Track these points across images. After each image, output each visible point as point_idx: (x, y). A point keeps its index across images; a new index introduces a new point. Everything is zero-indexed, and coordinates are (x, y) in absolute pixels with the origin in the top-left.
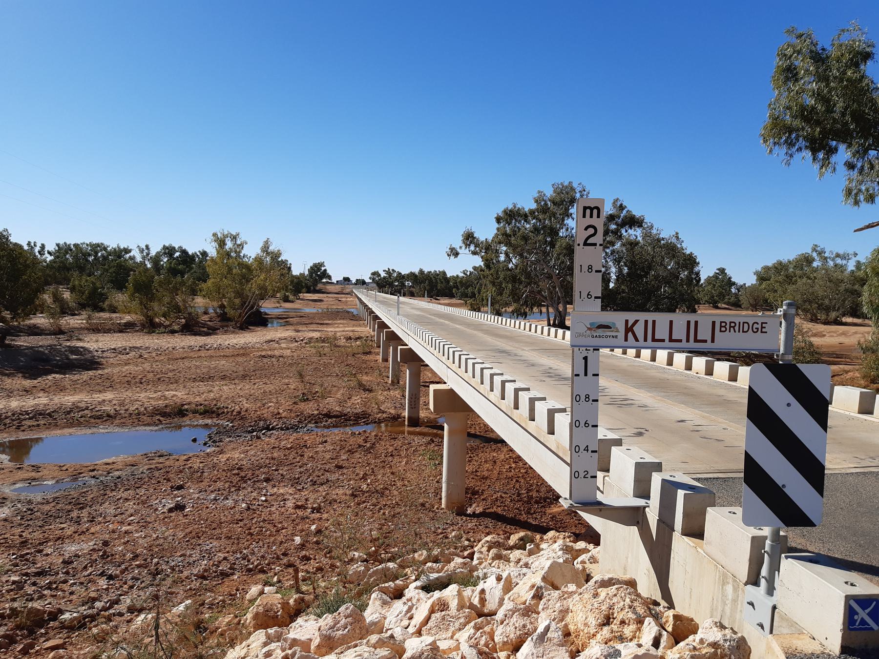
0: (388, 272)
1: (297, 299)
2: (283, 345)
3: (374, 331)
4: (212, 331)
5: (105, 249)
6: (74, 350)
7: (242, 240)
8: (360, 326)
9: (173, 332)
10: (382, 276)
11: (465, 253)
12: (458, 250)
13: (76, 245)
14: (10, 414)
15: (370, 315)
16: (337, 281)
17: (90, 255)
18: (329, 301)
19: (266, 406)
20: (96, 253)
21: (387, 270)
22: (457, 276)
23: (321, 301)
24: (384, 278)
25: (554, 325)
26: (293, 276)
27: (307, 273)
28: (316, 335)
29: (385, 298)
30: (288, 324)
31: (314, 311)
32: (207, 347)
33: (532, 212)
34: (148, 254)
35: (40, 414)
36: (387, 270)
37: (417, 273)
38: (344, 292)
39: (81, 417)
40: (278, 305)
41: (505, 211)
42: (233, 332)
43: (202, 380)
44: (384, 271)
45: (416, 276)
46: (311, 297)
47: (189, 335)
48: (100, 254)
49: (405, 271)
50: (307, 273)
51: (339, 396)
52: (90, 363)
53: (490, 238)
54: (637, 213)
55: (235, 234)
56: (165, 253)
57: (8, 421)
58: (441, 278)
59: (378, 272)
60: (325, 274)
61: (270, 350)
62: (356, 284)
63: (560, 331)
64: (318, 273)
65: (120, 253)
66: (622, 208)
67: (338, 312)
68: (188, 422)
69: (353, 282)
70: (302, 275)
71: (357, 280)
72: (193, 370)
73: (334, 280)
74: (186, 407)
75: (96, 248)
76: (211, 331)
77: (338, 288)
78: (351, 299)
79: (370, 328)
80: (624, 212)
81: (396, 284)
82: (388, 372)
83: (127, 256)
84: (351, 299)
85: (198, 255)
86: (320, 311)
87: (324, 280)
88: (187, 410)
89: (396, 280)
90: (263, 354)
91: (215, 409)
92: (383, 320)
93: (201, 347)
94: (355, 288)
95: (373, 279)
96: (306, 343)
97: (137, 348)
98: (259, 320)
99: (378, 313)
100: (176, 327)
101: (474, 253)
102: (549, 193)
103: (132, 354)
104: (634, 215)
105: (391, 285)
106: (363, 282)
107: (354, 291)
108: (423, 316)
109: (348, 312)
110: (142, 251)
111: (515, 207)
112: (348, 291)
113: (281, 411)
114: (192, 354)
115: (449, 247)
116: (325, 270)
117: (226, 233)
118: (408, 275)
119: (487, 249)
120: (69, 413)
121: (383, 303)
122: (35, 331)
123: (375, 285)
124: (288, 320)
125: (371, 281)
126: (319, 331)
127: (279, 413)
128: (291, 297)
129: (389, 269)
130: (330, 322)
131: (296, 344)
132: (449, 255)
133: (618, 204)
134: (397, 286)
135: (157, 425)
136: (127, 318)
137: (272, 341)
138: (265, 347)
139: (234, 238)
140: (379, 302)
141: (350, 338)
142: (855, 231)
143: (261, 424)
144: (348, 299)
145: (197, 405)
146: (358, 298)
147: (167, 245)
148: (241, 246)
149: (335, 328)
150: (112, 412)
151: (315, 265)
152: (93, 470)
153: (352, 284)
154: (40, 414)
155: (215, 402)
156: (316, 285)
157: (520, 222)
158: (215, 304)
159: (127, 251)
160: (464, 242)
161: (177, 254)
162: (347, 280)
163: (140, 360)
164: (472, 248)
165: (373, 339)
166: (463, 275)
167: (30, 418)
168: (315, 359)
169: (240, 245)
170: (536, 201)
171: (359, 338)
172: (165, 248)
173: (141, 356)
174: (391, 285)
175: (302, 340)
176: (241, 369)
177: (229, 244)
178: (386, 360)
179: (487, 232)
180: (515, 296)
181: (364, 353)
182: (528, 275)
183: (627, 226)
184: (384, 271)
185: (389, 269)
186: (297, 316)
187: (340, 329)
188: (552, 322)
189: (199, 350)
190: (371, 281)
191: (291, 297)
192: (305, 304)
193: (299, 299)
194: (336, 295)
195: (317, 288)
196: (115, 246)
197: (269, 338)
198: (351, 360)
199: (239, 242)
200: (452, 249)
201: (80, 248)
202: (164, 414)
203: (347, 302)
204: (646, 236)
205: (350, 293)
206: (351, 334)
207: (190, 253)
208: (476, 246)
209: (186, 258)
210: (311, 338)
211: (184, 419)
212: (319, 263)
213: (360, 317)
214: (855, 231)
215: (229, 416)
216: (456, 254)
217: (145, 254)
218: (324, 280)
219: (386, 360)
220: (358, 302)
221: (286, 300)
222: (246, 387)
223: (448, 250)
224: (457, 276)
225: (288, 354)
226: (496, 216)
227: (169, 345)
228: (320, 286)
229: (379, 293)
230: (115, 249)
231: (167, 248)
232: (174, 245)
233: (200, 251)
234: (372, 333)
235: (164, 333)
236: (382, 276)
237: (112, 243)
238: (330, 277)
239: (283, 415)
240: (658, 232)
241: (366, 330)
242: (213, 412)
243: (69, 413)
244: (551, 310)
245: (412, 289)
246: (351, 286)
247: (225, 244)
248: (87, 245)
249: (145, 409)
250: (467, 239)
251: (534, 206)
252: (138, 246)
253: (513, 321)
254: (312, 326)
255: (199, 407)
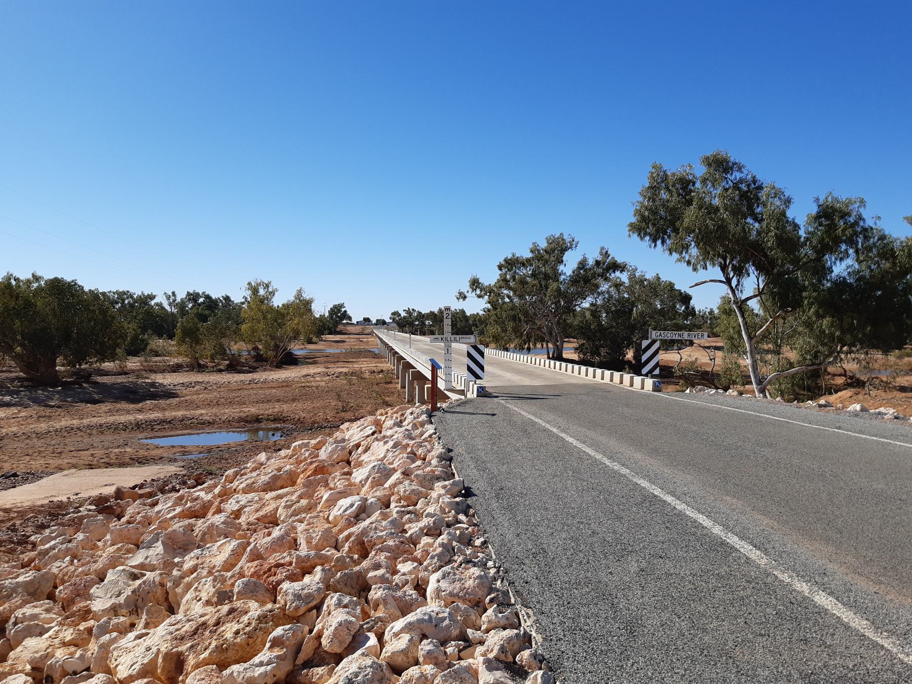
0: (408, 312)
1: (320, 341)
2: (318, 379)
3: (394, 366)
4: (253, 370)
5: (131, 297)
6: (153, 385)
7: (274, 287)
8: (382, 362)
9: (220, 371)
10: (402, 316)
11: (471, 296)
12: (466, 294)
13: (104, 294)
14: (144, 422)
15: (390, 352)
16: (357, 322)
17: (117, 303)
18: (351, 342)
19: (317, 415)
20: (123, 300)
21: (407, 309)
22: (478, 314)
23: (343, 342)
24: (405, 317)
25: (553, 358)
26: (271, 308)
27: (327, 314)
28: (345, 370)
29: (403, 337)
30: (315, 363)
31: (338, 351)
32: (255, 381)
33: (528, 260)
34: (174, 301)
35: (164, 422)
36: (407, 309)
37: (436, 312)
38: (365, 332)
39: (191, 423)
40: (303, 347)
41: (506, 260)
42: (271, 370)
43: (263, 402)
44: (404, 311)
45: (436, 315)
46: (333, 338)
47: (234, 373)
48: (126, 302)
49: (425, 311)
50: (328, 314)
51: (368, 408)
52: (168, 394)
53: (493, 283)
54: (620, 260)
55: (267, 282)
56: (190, 300)
57: (144, 426)
58: (461, 316)
59: (398, 312)
60: (345, 315)
61: (308, 382)
62: (376, 324)
63: (558, 363)
64: (338, 315)
65: (145, 300)
66: (607, 255)
67: (360, 351)
68: (264, 426)
69: (373, 322)
70: (322, 316)
71: (377, 320)
72: (253, 396)
73: (354, 321)
74: (261, 417)
75: (122, 295)
76: (251, 370)
77: (358, 329)
78: (372, 339)
79: (391, 364)
80: (610, 258)
81: (417, 323)
82: (405, 395)
83: (153, 303)
84: (372, 339)
85: (221, 301)
86: (344, 351)
87: (345, 321)
88: (262, 419)
89: (417, 319)
90: (303, 385)
91: (281, 418)
92: (401, 354)
93: (250, 381)
94: (376, 329)
95: (394, 319)
96: (337, 377)
97: (200, 382)
98: (291, 360)
99: (397, 350)
100: (222, 367)
101: (479, 296)
102: (543, 245)
103: (197, 387)
104: (616, 261)
105: (411, 324)
106: (383, 323)
107: (375, 331)
108: (431, 350)
109: (370, 352)
110: (168, 298)
111: (513, 255)
112: (368, 331)
113: (329, 418)
114: (245, 387)
115: (458, 291)
116: (345, 311)
117: (259, 281)
118: (428, 314)
119: (490, 292)
120: (182, 421)
121: (402, 341)
122: (106, 373)
123: (396, 325)
124: (315, 359)
125: (391, 321)
126: (347, 367)
127: (327, 419)
128: (314, 339)
129: (409, 309)
130: (354, 360)
131: (328, 378)
132: (458, 299)
133: (604, 251)
134: (417, 325)
135: (244, 428)
136: (174, 361)
137: (308, 375)
138: (303, 380)
139: (267, 286)
140: (398, 340)
141: (374, 372)
142: (690, 287)
143: (316, 425)
144: (369, 339)
145: (268, 416)
146: (381, 339)
147: (191, 292)
148: (273, 293)
149: (359, 364)
150: (211, 420)
151: (335, 307)
152: (219, 447)
153: (372, 325)
154: (164, 422)
155: (280, 413)
156: (337, 327)
157: (519, 268)
158: (250, 347)
159: (152, 297)
160: (471, 288)
161: (201, 300)
162: (367, 320)
163: (206, 391)
164: (478, 292)
165: (393, 372)
166: (483, 312)
167: (158, 424)
168: (347, 387)
169: (271, 292)
170: (532, 251)
171: (382, 371)
172: (189, 294)
173: (206, 388)
174: (411, 324)
175: (333, 374)
176: (290, 395)
177: (262, 292)
178: (403, 387)
179: (491, 277)
180: (517, 331)
181: (386, 383)
182: (526, 314)
183: (611, 271)
184: (404, 311)
185: (409, 309)
186: (323, 356)
187: (365, 365)
188: (551, 356)
189: (249, 384)
190: (391, 321)
191: (314, 339)
192: (327, 345)
193: (322, 340)
194: (357, 336)
195: (338, 330)
196: (140, 294)
197: (304, 373)
198: (375, 388)
199: (270, 290)
200: (460, 293)
201: (108, 296)
202: (247, 422)
203: (368, 342)
204: (632, 278)
205: (371, 334)
206: (374, 369)
207: (214, 298)
208: (481, 291)
209: (211, 303)
210: (341, 373)
211: (262, 424)
212: (339, 304)
213: (381, 356)
214: (690, 287)
215: (292, 421)
216: (465, 298)
217: (171, 301)
218: (345, 321)
219: (403, 387)
220: (379, 342)
221: (310, 342)
222: (299, 405)
223: (457, 294)
224: (478, 314)
225: (324, 385)
226: (498, 264)
227: (224, 380)
228: (340, 327)
229: (399, 333)
230: (140, 297)
231: (191, 294)
232: (197, 291)
233: (223, 297)
234: (393, 368)
235: (213, 371)
236: (402, 316)
237: (137, 290)
238: (350, 318)
239: (330, 420)
240: (643, 274)
241: (388, 365)
242: (281, 420)
243: (182, 421)
244: (550, 345)
245: (432, 328)
246: (372, 327)
247: (258, 292)
248: (114, 293)
249: (233, 418)
250: (473, 285)
251: (530, 255)
252: (165, 293)
253: (515, 355)
254: (339, 363)
255: (270, 417)
